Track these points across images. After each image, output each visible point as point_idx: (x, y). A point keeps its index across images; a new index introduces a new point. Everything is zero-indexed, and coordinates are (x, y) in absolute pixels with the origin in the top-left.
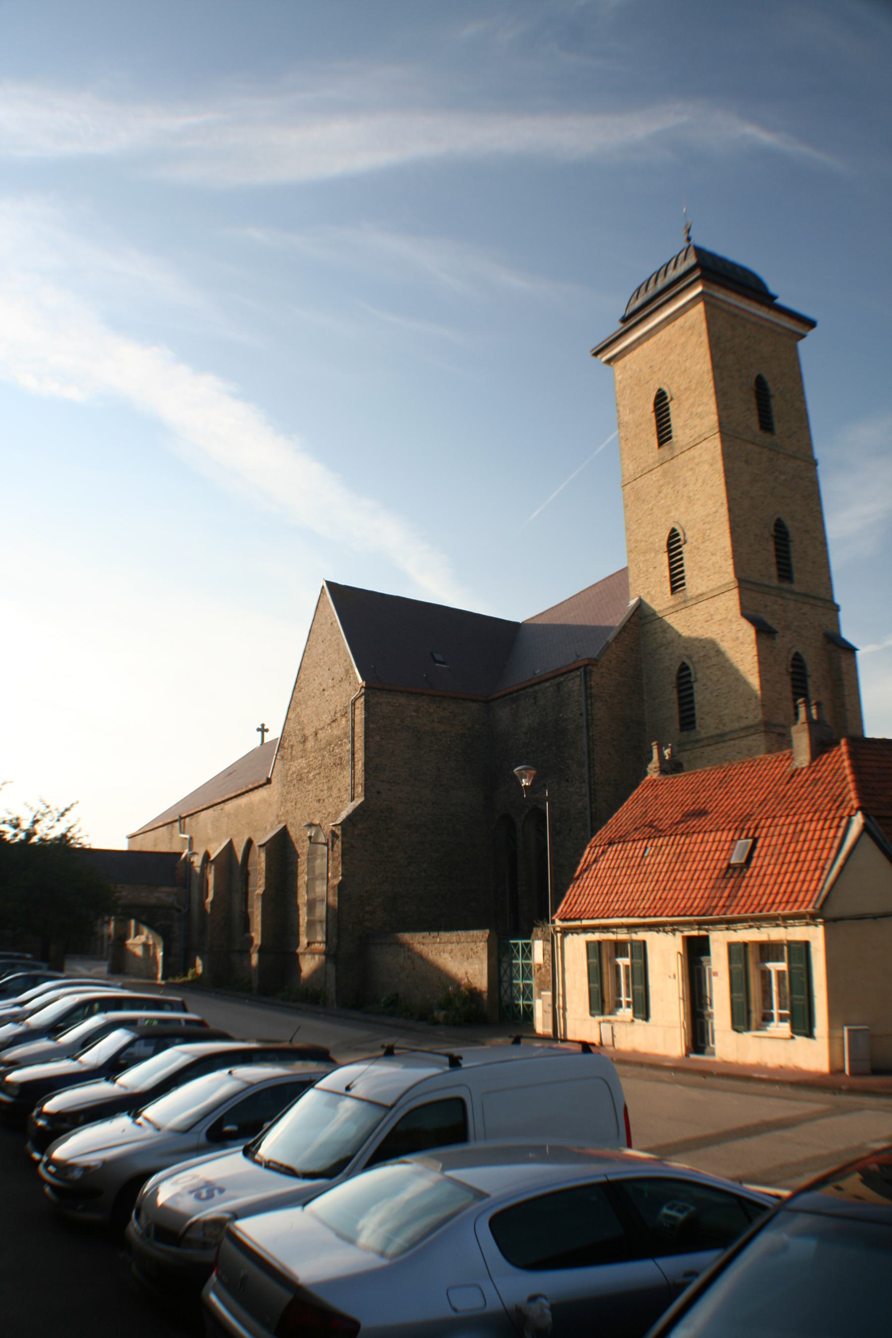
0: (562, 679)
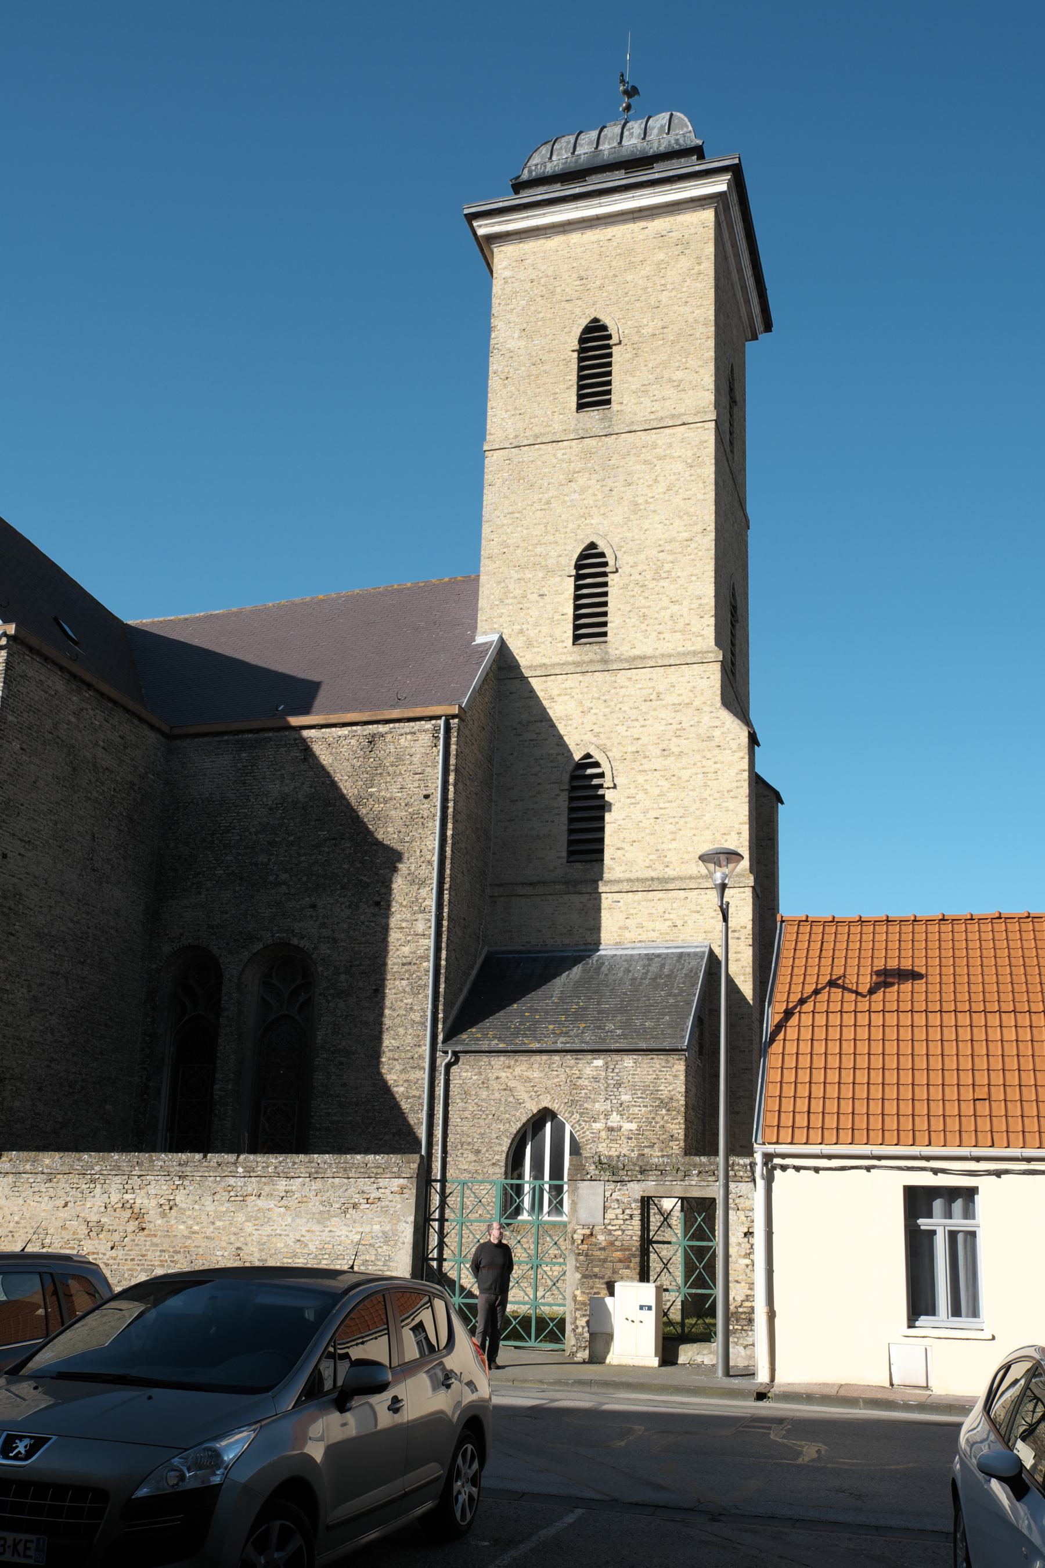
0: (382, 729)
